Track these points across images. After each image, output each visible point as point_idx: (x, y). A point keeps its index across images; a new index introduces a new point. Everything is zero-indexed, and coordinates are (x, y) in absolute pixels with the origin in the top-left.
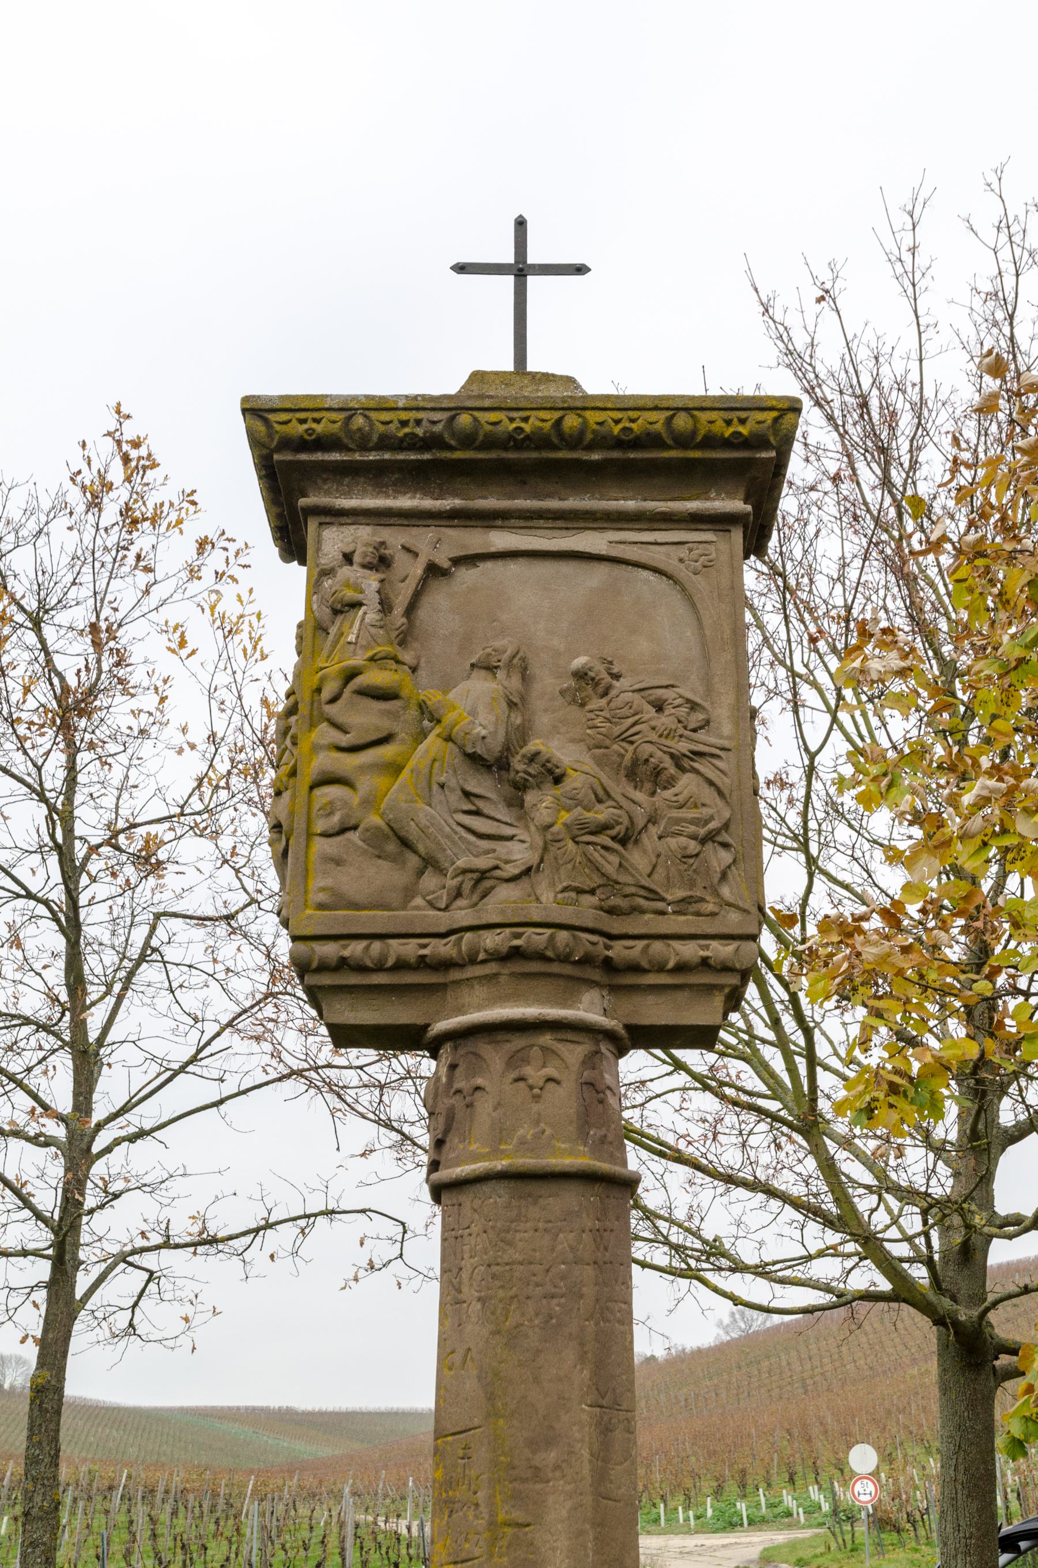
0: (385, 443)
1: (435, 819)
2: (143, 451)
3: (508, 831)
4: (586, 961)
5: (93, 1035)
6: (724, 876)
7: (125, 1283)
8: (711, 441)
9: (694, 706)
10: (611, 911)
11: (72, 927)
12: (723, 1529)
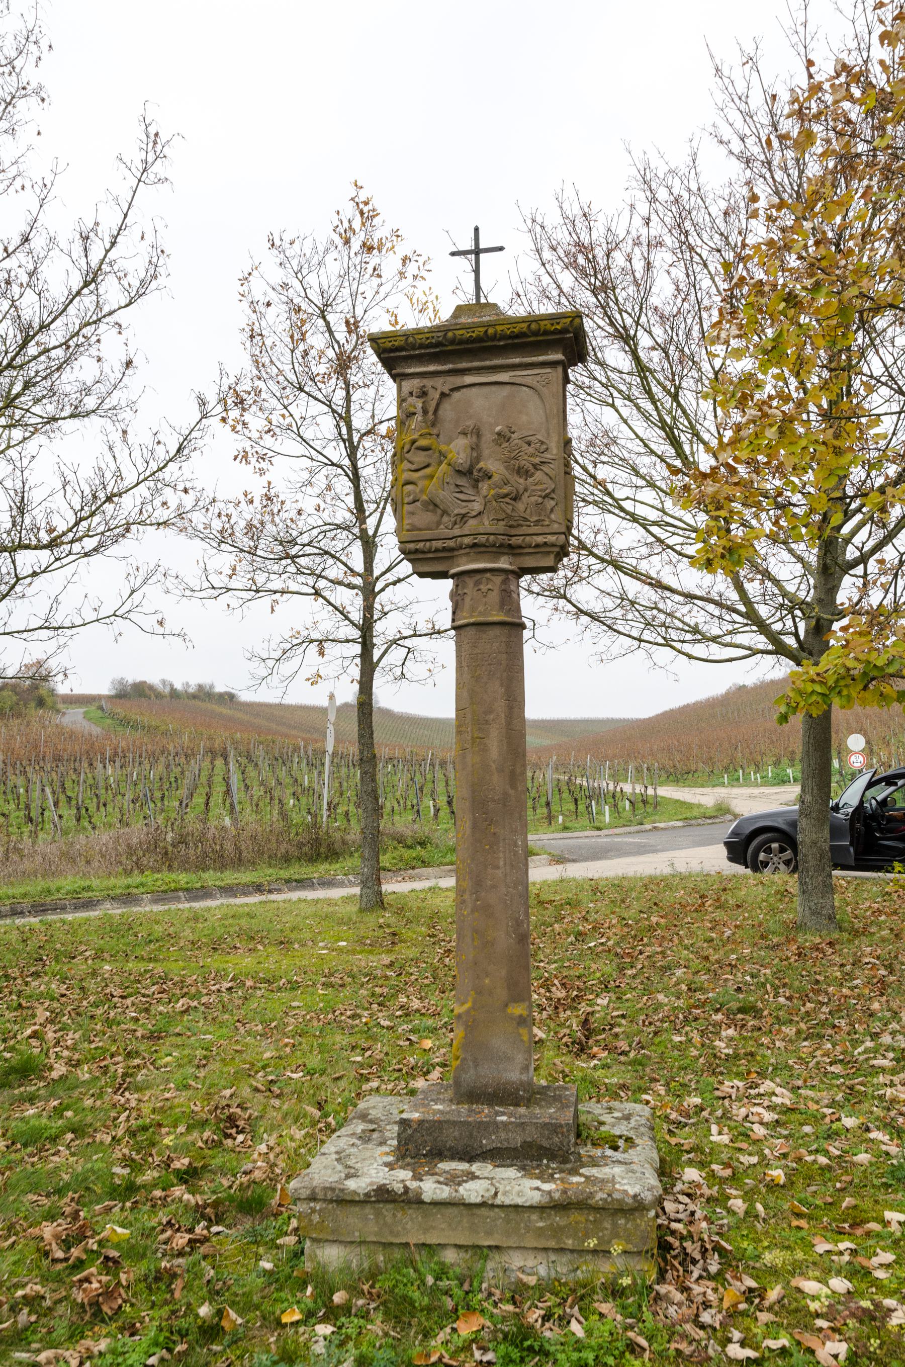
0: (422, 346)
1: (446, 496)
2: (370, 207)
3: (473, 498)
4: (501, 546)
5: (371, 532)
6: (552, 510)
7: (396, 655)
8: (546, 333)
9: (542, 443)
10: (511, 526)
11: (356, 479)
12: (778, 784)
